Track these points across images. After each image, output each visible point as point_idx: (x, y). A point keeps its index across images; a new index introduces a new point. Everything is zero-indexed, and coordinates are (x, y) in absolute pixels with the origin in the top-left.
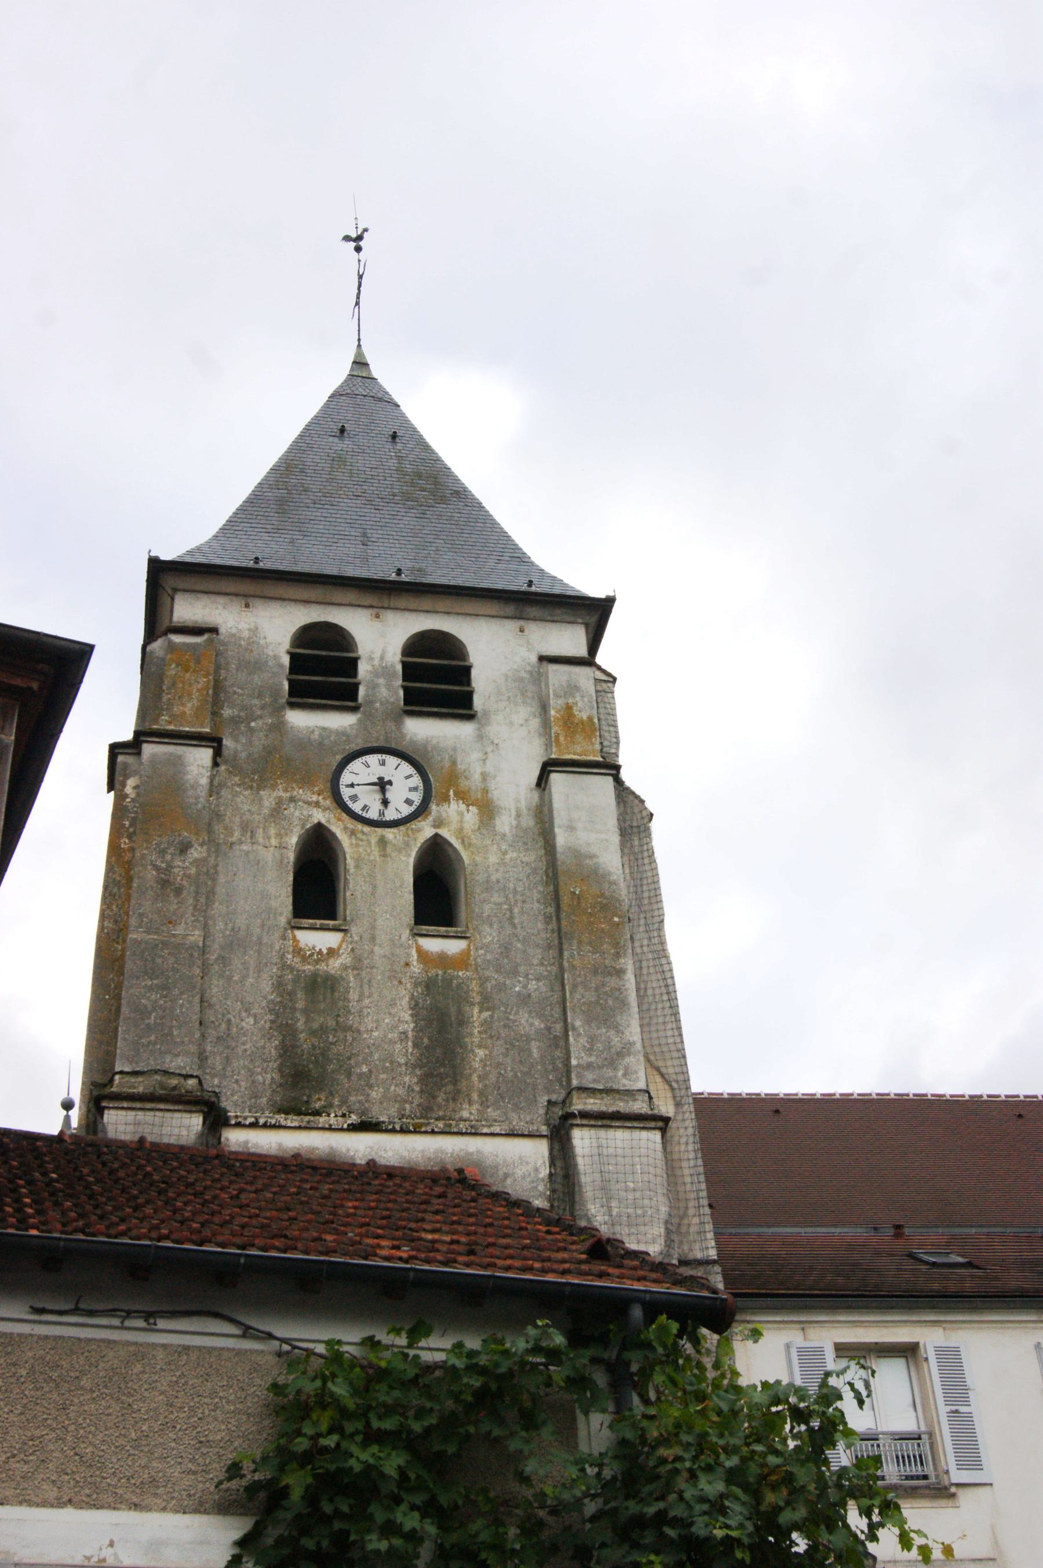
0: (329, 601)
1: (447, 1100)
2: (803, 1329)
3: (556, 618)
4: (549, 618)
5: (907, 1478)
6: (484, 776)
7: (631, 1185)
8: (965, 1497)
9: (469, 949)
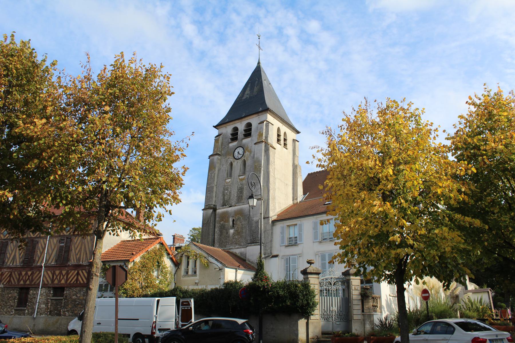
8: (299, 246)
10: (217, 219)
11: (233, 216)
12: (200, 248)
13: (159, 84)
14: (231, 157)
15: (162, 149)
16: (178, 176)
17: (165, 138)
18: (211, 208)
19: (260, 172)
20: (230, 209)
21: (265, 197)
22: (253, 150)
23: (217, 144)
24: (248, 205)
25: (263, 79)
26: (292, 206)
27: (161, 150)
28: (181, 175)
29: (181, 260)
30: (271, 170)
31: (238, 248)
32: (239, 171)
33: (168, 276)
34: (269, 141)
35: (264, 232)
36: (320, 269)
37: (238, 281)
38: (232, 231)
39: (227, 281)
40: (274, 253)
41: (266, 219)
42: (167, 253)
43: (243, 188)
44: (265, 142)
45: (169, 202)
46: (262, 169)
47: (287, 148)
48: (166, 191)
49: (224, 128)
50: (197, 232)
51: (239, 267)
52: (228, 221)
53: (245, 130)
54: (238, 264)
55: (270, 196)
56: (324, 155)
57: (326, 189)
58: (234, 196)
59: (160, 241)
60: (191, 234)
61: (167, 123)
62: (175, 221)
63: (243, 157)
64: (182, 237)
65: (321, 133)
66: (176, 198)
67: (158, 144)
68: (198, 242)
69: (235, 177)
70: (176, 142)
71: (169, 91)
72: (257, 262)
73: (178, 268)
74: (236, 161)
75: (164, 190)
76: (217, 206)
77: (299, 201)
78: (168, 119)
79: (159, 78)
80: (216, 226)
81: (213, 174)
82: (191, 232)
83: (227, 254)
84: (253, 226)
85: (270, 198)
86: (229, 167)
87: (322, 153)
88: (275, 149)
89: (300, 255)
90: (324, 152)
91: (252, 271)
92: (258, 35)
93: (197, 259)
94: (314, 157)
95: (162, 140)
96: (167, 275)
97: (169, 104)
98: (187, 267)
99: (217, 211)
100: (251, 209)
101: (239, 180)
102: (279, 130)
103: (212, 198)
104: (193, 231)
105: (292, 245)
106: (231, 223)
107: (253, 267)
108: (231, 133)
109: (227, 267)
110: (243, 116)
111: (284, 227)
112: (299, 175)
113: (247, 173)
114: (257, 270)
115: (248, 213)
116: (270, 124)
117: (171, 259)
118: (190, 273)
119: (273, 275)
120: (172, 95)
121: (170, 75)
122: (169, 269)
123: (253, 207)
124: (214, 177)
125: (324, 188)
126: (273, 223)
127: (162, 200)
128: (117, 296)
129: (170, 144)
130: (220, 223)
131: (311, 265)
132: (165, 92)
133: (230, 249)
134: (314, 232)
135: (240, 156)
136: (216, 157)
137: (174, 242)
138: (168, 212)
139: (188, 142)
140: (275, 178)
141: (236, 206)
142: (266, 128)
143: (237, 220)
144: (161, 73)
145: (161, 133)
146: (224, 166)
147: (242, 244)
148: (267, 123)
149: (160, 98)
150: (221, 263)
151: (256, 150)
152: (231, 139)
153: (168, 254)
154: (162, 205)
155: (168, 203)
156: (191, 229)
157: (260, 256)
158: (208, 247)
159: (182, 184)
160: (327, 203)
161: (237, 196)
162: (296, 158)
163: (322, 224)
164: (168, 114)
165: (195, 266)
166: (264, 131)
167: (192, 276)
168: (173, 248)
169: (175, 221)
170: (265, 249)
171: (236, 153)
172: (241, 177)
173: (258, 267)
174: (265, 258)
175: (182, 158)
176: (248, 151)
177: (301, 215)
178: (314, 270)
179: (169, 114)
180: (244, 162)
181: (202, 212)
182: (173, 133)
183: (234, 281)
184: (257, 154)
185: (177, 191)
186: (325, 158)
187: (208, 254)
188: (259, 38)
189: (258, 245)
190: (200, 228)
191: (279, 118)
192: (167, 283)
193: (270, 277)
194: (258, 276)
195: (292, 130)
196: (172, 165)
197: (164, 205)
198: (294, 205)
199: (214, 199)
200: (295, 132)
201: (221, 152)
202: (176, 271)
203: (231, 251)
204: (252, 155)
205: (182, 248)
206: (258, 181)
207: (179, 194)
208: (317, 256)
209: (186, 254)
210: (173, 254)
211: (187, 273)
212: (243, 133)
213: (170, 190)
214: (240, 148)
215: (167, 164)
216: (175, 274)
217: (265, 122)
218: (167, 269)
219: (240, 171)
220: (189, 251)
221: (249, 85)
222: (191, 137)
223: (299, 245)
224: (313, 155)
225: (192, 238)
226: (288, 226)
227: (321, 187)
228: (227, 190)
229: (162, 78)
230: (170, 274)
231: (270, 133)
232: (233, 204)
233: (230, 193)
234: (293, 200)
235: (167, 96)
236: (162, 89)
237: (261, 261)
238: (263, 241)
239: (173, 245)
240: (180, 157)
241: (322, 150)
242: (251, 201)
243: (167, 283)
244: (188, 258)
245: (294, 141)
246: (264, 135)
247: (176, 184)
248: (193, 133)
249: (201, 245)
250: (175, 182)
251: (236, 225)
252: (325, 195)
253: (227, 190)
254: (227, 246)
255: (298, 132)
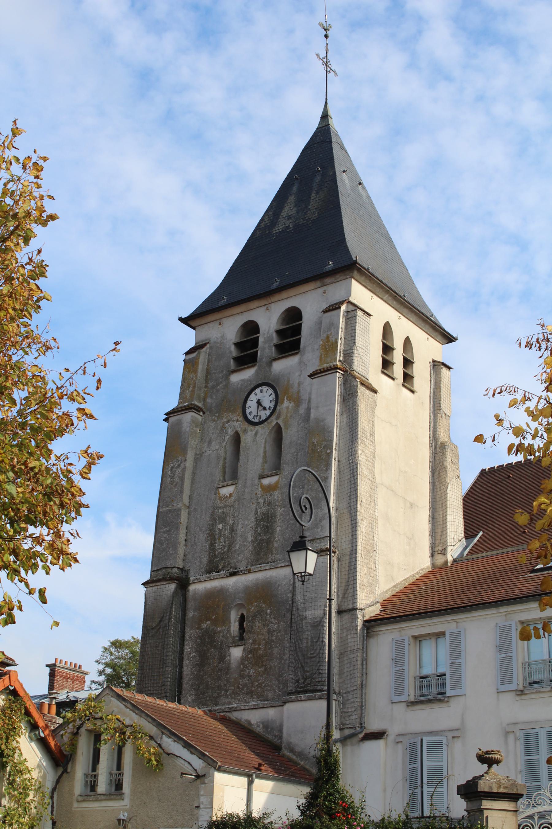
0: (249, 309)
1: (264, 555)
2: (400, 631)
3: (338, 280)
4: (336, 281)
5: (421, 696)
6: (299, 384)
7: (314, 583)
8: (453, 702)
9: (279, 480)
10: (191, 614)
11: (241, 606)
12: (135, 708)
13: (10, 186)
14: (237, 416)
15: (19, 395)
16: (70, 481)
17: (29, 360)
18: (170, 579)
19: (328, 466)
20: (231, 582)
21: (346, 547)
22: (305, 397)
23: (192, 375)
24: (288, 570)
25: (338, 168)
26: (429, 573)
27: (15, 396)
28: (76, 478)
29: (73, 746)
30: (362, 457)
31: (256, 708)
32: (260, 460)
33: (31, 797)
34: (358, 367)
35: (341, 655)
36: (520, 780)
37: (255, 815)
38: (236, 653)
39: (219, 815)
40: (373, 726)
41: (346, 617)
42: (29, 722)
43: (274, 516)
44: (345, 371)
45: (40, 564)
46: (335, 455)
47: (415, 388)
48: (31, 529)
49: (215, 325)
50: (126, 652)
51: (259, 769)
52: (226, 621)
53: (280, 333)
54: (255, 760)
55: (359, 540)
56: (533, 415)
57: (540, 524)
58: (246, 539)
59: (7, 683)
60: (108, 658)
61: (33, 313)
62: (57, 624)
63: (272, 418)
64: (77, 668)
65: (524, 344)
66: (62, 552)
67: (7, 378)
68: (128, 685)
69: (249, 482)
70: (64, 373)
71: (41, 210)
72: (318, 754)
73: (65, 771)
74: (251, 431)
75: (23, 525)
76: (192, 573)
77: (450, 559)
78: (38, 300)
79: (8, 169)
80: (187, 637)
81: (178, 471)
82: (107, 654)
83: (220, 726)
84: (305, 635)
85: (359, 548)
86: (230, 449)
87: (527, 410)
88: (375, 391)
89: (455, 734)
90: (531, 405)
91: (300, 783)
92: (321, 25)
93: (124, 741)
94: (500, 421)
95: (17, 366)
96: (27, 795)
97: (39, 251)
98: (94, 769)
99: (192, 588)
100: (298, 584)
101: (260, 491)
102: (387, 330)
103: (175, 549)
104: (113, 650)
105: (429, 701)
106: (234, 627)
107: (304, 769)
108: (238, 340)
109: (219, 770)
110: (275, 286)
111: (403, 641)
112: (450, 473)
113: (286, 469)
114: (317, 780)
115: (290, 595)
116: (359, 313)
117: (43, 743)
118: (102, 787)
119: (368, 798)
120: (50, 223)
121: (45, 159)
122: (35, 774)
123: (304, 577)
124: (182, 479)
125: (533, 519)
126: (368, 628)
127: (16, 555)
128: (356, 609)
129: (43, 378)
130: (199, 628)
131: (490, 766)
132: (29, 214)
133: (230, 710)
134: (501, 659)
135: (264, 415)
136: (188, 417)
137: (51, 686)
138: (36, 595)
139: (101, 372)
140: (374, 485)
141: (250, 572)
142: (347, 324)
143: (254, 617)
144: (14, 152)
145: (14, 345)
146: (215, 446)
147: (270, 695)
148: (351, 308)
149: (12, 233)
150: (202, 756)
151: (313, 396)
152: (235, 359)
153: (34, 727)
154: (16, 572)
155: (35, 567)
156: (107, 644)
157: (328, 737)
158: (159, 702)
159: (81, 505)
160: (540, 566)
161: (253, 542)
162: (442, 422)
163: (525, 636)
164: (37, 282)
165: (119, 766)
166: (341, 335)
167: (108, 796)
168: (50, 705)
169: (57, 624)
170: (343, 713)
171: (252, 403)
172: (266, 482)
173: (320, 770)
174: (344, 740)
175: (82, 424)
176: (289, 399)
177: (460, 602)
178: (499, 784)
179: (41, 282)
180: (278, 432)
181: (143, 590)
182: (53, 344)
183: (242, 815)
184: (317, 407)
185: (65, 528)
186: (534, 425)
187: (159, 725)
188: (326, 36)
189: (320, 698)
190: (137, 641)
191: (387, 292)
192: (26, 820)
193: (357, 803)
194: (320, 800)
195: (430, 331)
196: (50, 447)
197: (23, 573)
198: (436, 569)
199: (181, 550)
200: (439, 338)
201: (204, 400)
202: (58, 782)
203: (235, 716)
204: (302, 410)
205: (79, 706)
206: (321, 495)
207: (71, 538)
208: (511, 738)
209: (89, 725)
210: (47, 727)
211: (93, 787)
212: (275, 340)
213: (42, 524)
214: (265, 388)
215: (33, 443)
216: (54, 790)
217: (344, 307)
218: (27, 776)
219: (265, 462)
220: (100, 715)
221: (295, 189)
222: (110, 358)
223: (452, 700)
224: (497, 417)
225: (109, 671)
226: (415, 638)
227: (522, 519)
228: (223, 520)
229: (16, 169)
230: (36, 791)
231: (359, 340)
232: (242, 567)
233: (232, 530)
234: (432, 556)
235: (34, 225)
236: (16, 202)
237: (329, 752)
238: (335, 686)
239: (50, 695)
240: (75, 421)
241: (526, 399)
242: (297, 558)
243: (26, 820)
244: (97, 737)
245: (437, 365)
246: (340, 348)
247: (62, 506)
248: (117, 343)
249: (139, 697)
250: (57, 501)
251: (250, 632)
252: (535, 544)
253: (223, 520)
254: (223, 700)
255: (449, 339)
